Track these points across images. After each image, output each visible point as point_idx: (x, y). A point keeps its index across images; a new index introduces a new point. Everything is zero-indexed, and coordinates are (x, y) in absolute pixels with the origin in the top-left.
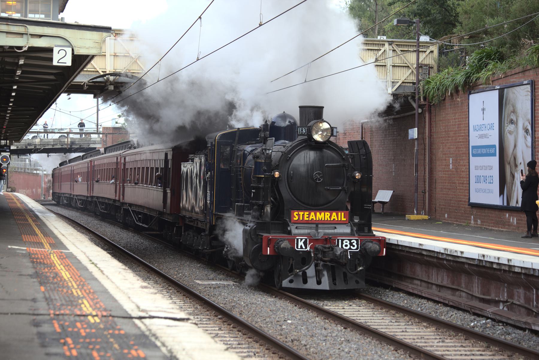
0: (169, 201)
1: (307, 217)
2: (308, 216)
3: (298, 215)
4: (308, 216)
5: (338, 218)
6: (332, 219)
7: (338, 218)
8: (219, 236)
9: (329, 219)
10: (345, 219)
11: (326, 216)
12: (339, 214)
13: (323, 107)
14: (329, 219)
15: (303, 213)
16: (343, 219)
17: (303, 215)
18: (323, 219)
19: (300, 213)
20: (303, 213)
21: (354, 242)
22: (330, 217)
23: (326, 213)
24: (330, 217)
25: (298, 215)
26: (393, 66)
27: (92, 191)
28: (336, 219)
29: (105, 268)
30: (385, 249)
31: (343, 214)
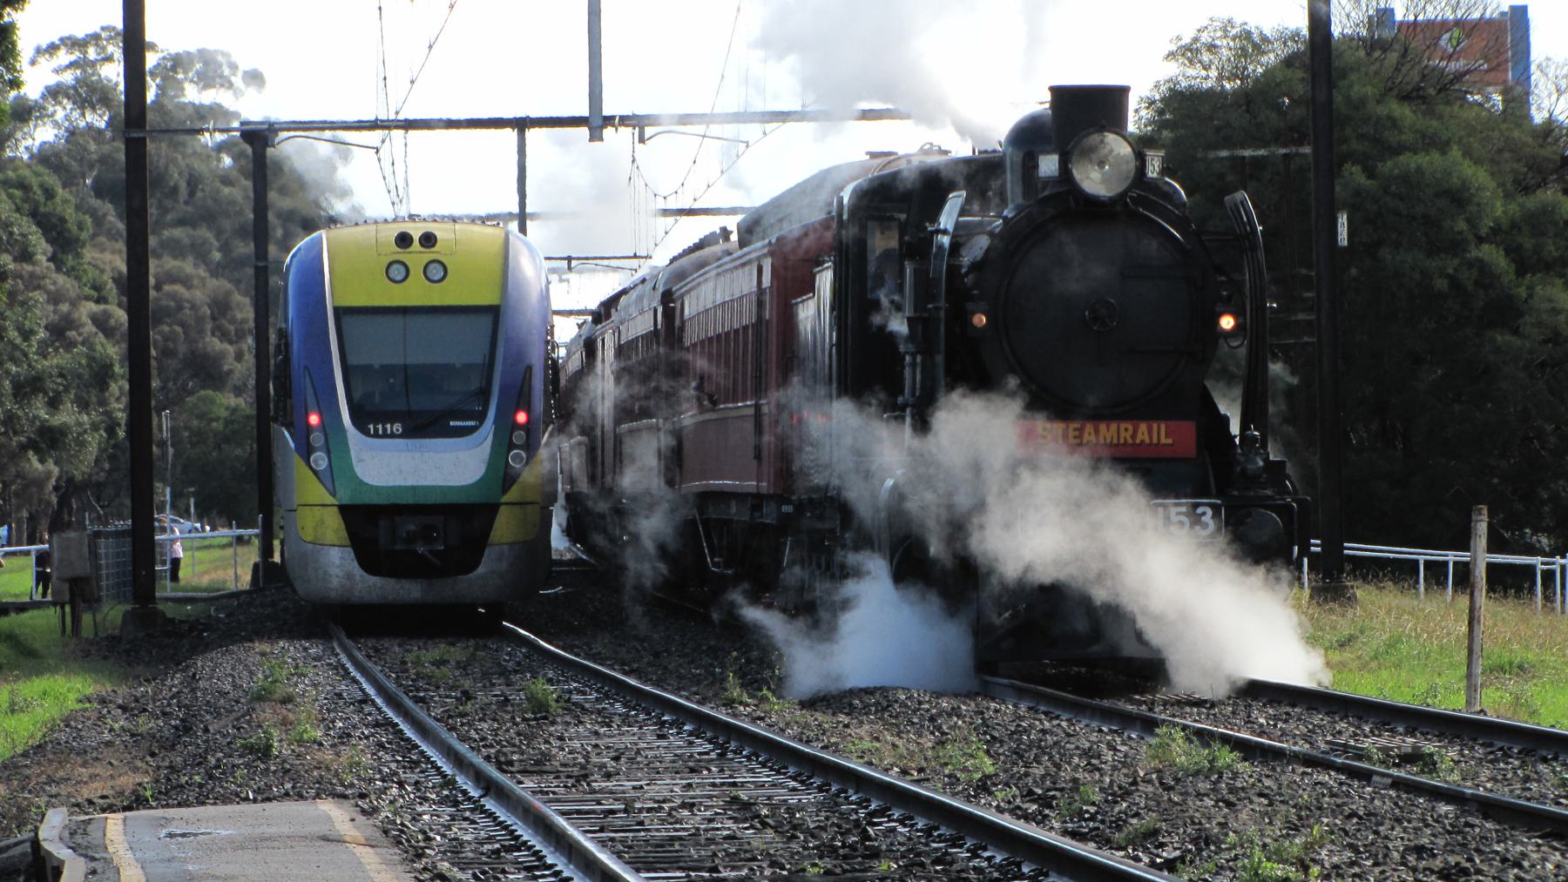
0: (918, 386)
2: (1077, 433)
4: (1077, 433)
5: (1151, 438)
6: (1138, 441)
7: (1151, 438)
8: (673, 384)
9: (1130, 441)
10: (1170, 441)
11: (1123, 434)
12: (1155, 426)
13: (590, 140)
14: (1130, 441)
16: (1164, 440)
21: (1204, 514)
22: (1134, 436)
23: (1123, 425)
24: (1134, 436)
26: (546, 258)
27: (843, 292)
28: (1147, 441)
29: (420, 252)
30: (1296, 548)
31: (1163, 427)
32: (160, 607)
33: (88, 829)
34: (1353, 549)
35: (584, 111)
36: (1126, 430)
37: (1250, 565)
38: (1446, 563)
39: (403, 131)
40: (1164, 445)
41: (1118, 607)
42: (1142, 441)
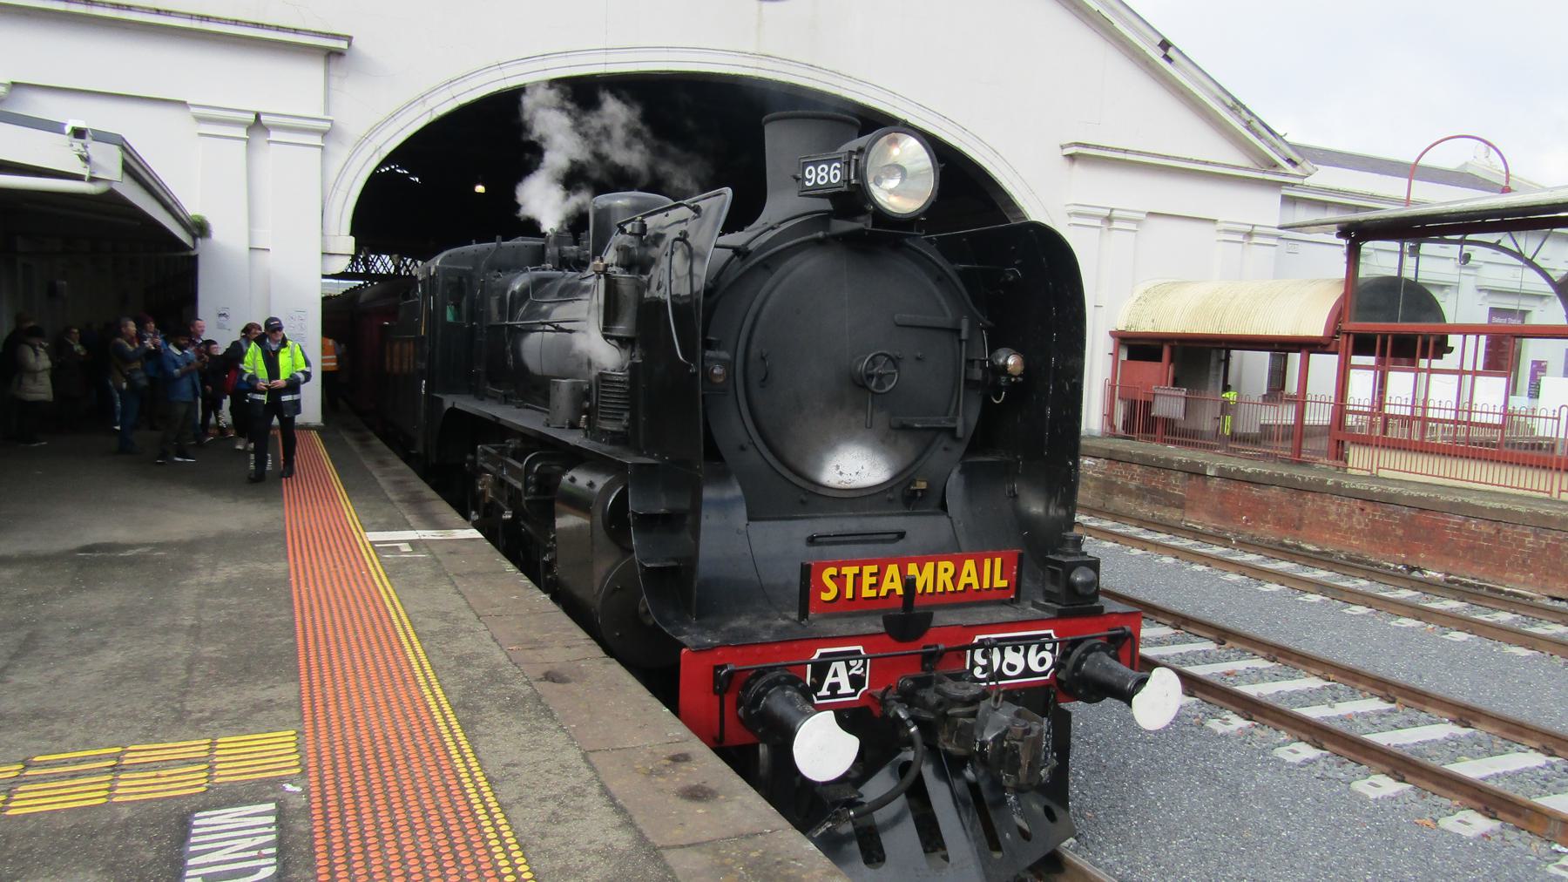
1: (871, 586)
3: (839, 579)
4: (873, 580)
6: (960, 587)
9: (950, 588)
10: (1004, 584)
11: (942, 576)
15: (856, 570)
17: (858, 577)
19: (845, 570)
20: (856, 570)
22: (955, 578)
23: (1311, 423)
24: (955, 578)
25: (839, 579)
28: (976, 586)
30: (424, 382)
32: (700, 284)
33: (293, 709)
34: (1378, 372)
35: (1456, 377)
36: (946, 570)
37: (630, 166)
38: (1402, 321)
39: (1459, 246)
40: (998, 589)
41: (539, 223)
42: (968, 586)
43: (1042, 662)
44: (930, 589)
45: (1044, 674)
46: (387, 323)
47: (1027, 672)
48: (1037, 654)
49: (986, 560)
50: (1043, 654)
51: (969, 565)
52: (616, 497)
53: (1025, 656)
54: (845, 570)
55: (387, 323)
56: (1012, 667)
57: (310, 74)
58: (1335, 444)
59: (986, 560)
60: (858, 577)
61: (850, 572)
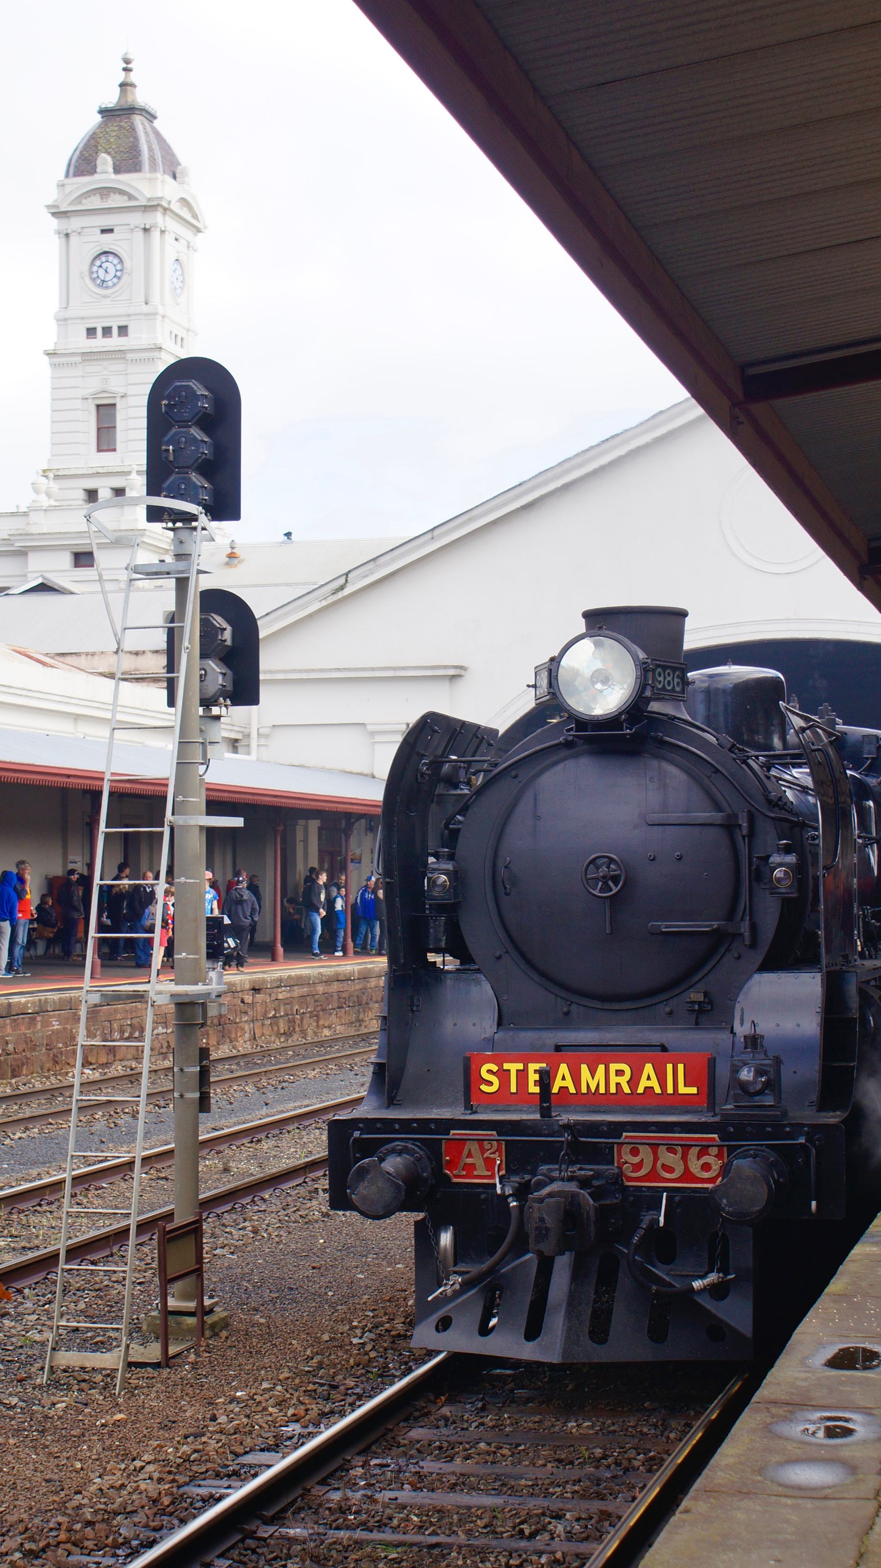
3: (503, 1075)
5: (663, 1083)
6: (640, 1090)
7: (663, 1083)
9: (627, 1090)
10: (693, 1090)
11: (614, 1079)
12: (670, 1067)
14: (627, 1090)
15: (520, 1066)
16: (682, 1090)
17: (522, 1075)
18: (584, 1068)
22: (634, 1082)
23: (614, 1067)
24: (634, 1082)
25: (503, 1075)
31: (681, 1067)
43: (706, 1167)
44: (602, 1090)
45: (711, 1180)
46: (814, 1204)
47: (687, 1175)
48: (699, 1158)
49: (695, 1089)
50: (705, 1159)
51: (649, 1069)
52: (667, 1200)
53: (684, 1158)
54: (506, 1066)
55: (814, 1204)
56: (669, 1169)
57: (143, 299)
58: (64, 239)
59: (695, 1089)
60: (522, 1075)
61: (513, 1067)
